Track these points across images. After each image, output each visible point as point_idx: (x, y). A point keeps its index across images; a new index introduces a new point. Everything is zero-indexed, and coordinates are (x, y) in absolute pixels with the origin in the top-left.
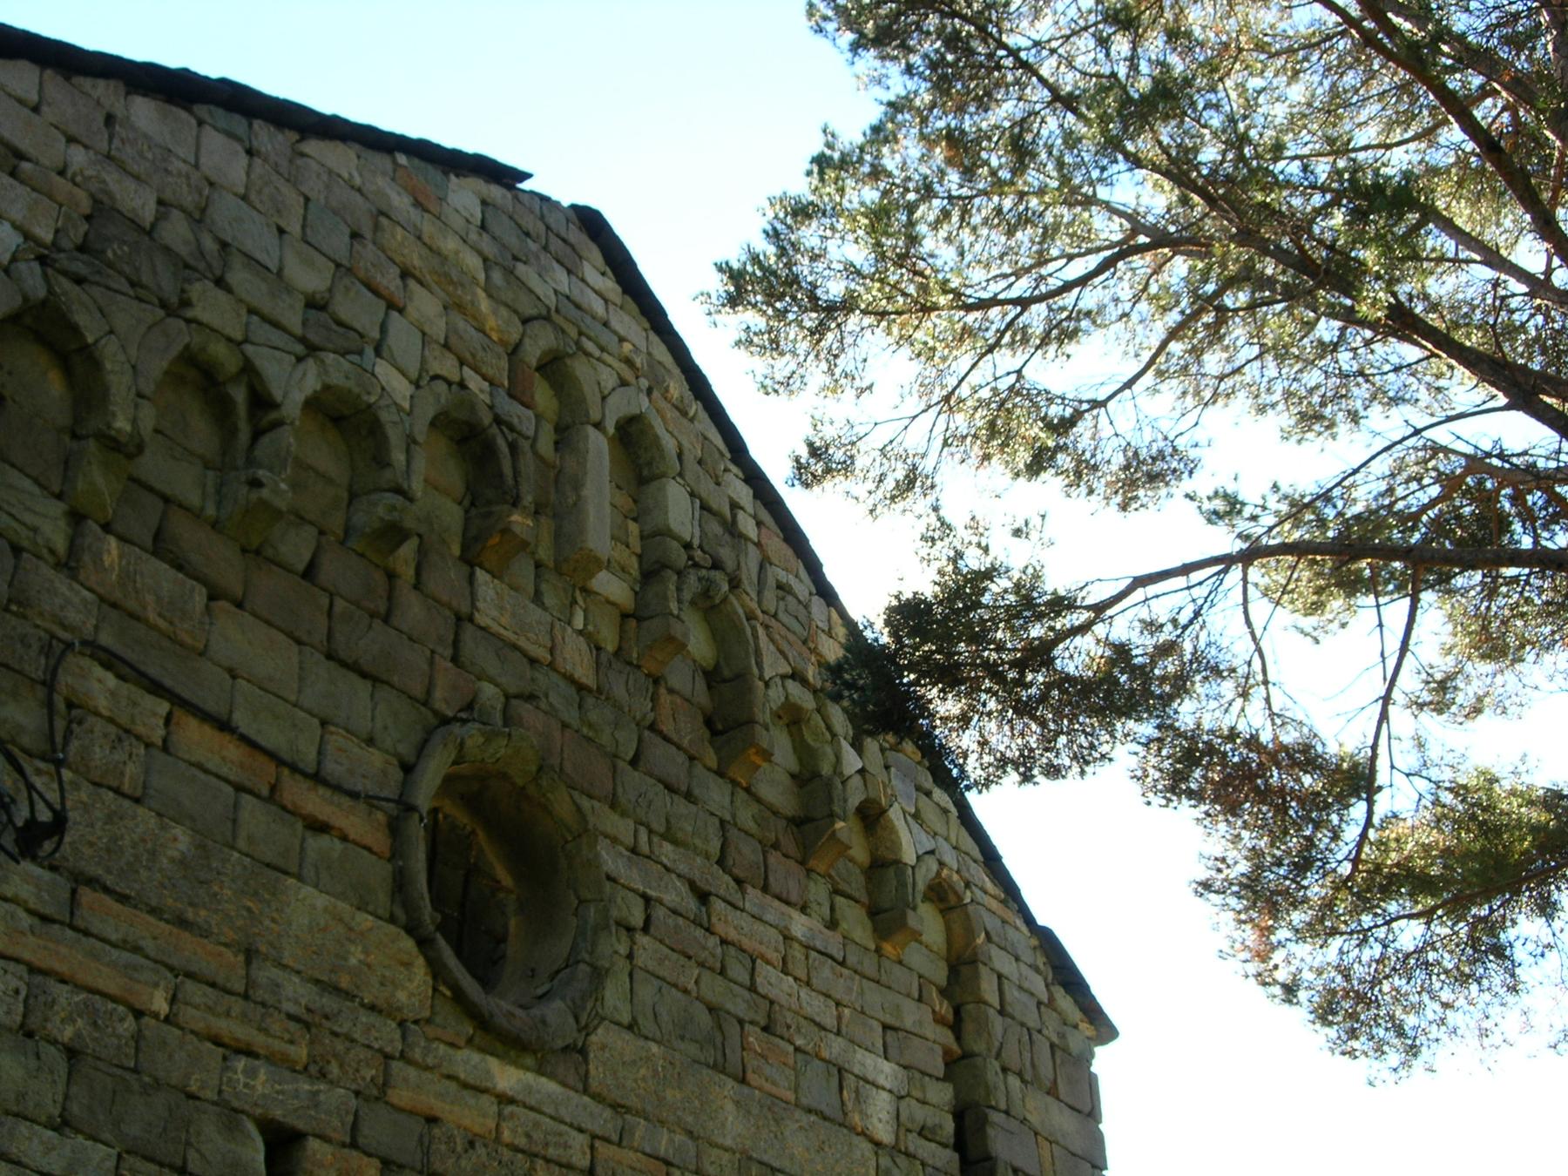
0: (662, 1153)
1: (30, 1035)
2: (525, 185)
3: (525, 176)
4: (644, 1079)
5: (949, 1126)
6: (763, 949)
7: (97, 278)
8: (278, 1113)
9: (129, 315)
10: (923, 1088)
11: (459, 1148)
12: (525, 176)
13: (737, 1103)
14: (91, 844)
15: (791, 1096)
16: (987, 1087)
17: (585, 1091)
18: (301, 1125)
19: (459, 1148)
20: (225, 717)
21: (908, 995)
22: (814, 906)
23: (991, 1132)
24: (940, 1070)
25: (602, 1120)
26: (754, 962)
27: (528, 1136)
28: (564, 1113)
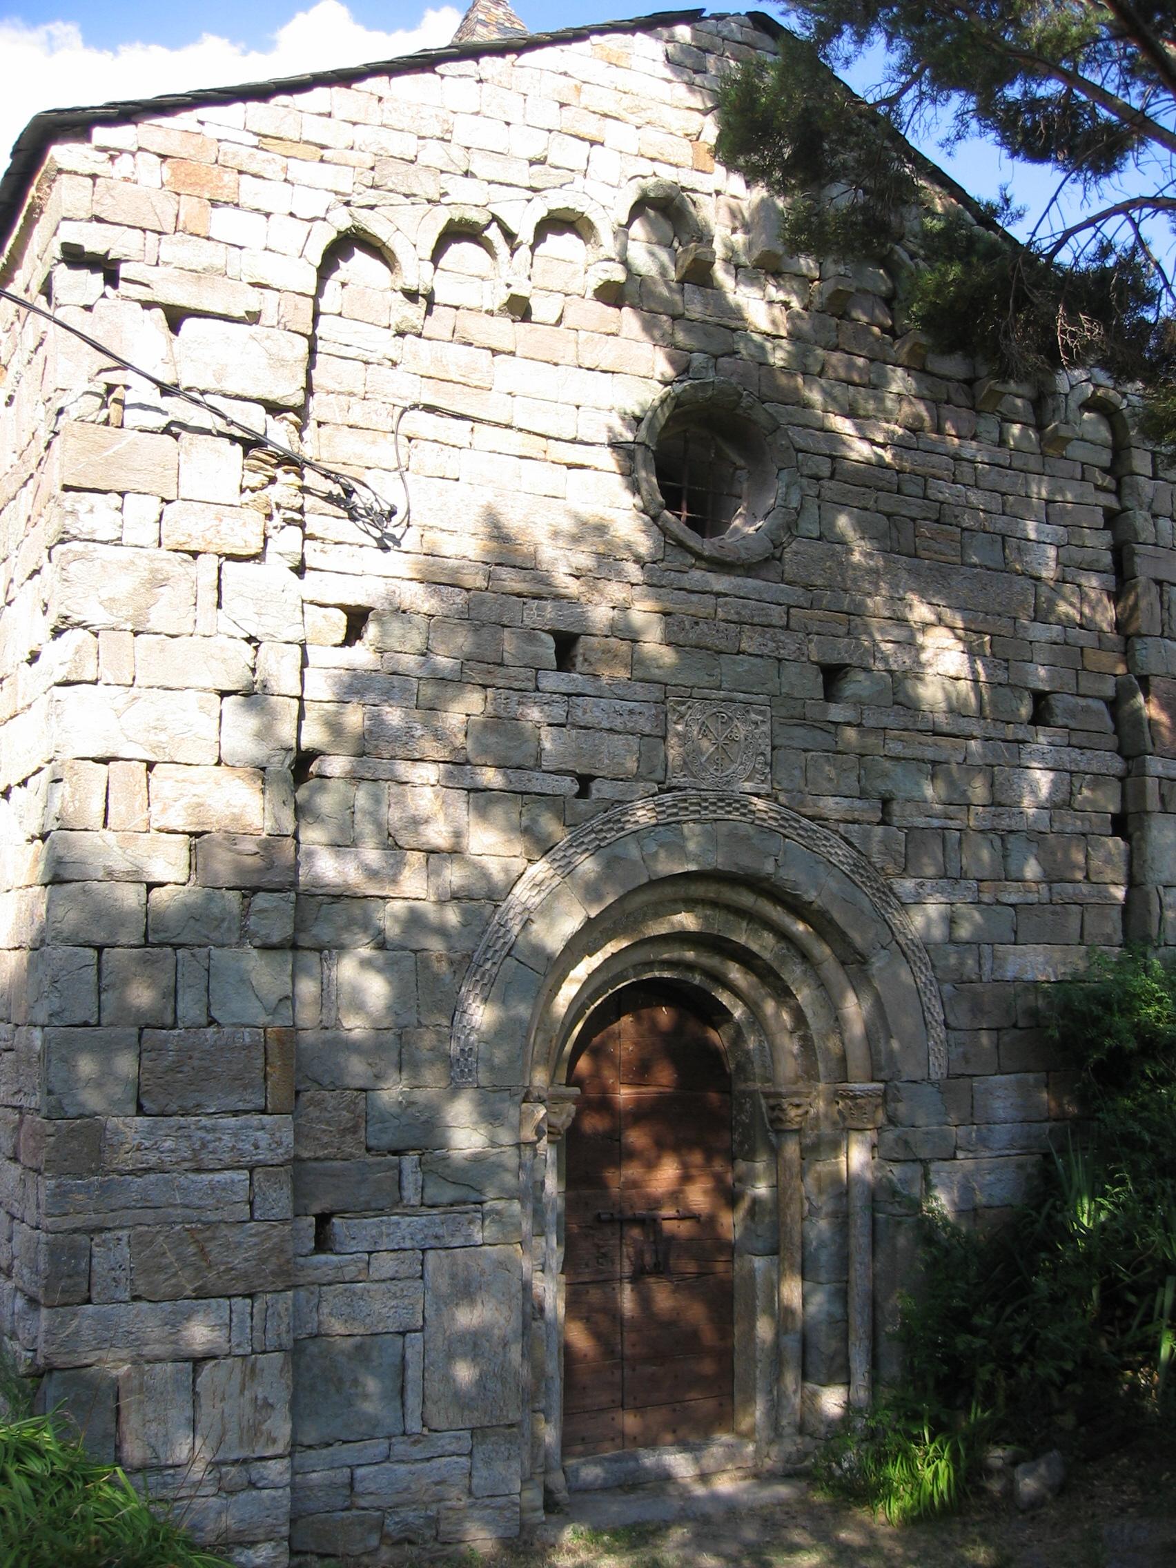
0: (845, 608)
1: (250, 639)
2: (705, 14)
3: (703, 10)
4: (830, 568)
5: (1107, 558)
6: (934, 471)
7: (384, 202)
8: (561, 627)
9: (407, 214)
10: (1081, 536)
11: (688, 627)
12: (703, 10)
13: (909, 571)
14: (430, 510)
15: (957, 560)
16: (1135, 530)
17: (782, 581)
18: (576, 630)
19: (688, 627)
20: (262, 433)
21: (1073, 478)
22: (985, 435)
23: (1137, 559)
24: (1100, 522)
25: (796, 595)
26: (926, 481)
27: (738, 613)
28: (765, 596)
